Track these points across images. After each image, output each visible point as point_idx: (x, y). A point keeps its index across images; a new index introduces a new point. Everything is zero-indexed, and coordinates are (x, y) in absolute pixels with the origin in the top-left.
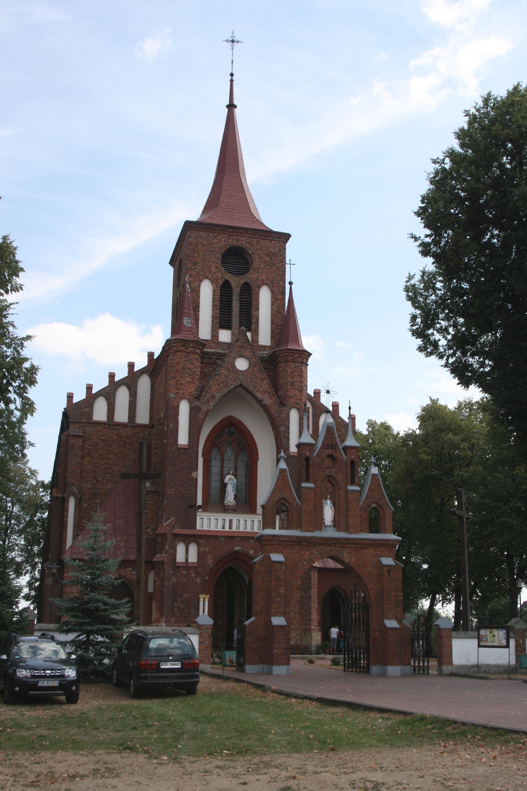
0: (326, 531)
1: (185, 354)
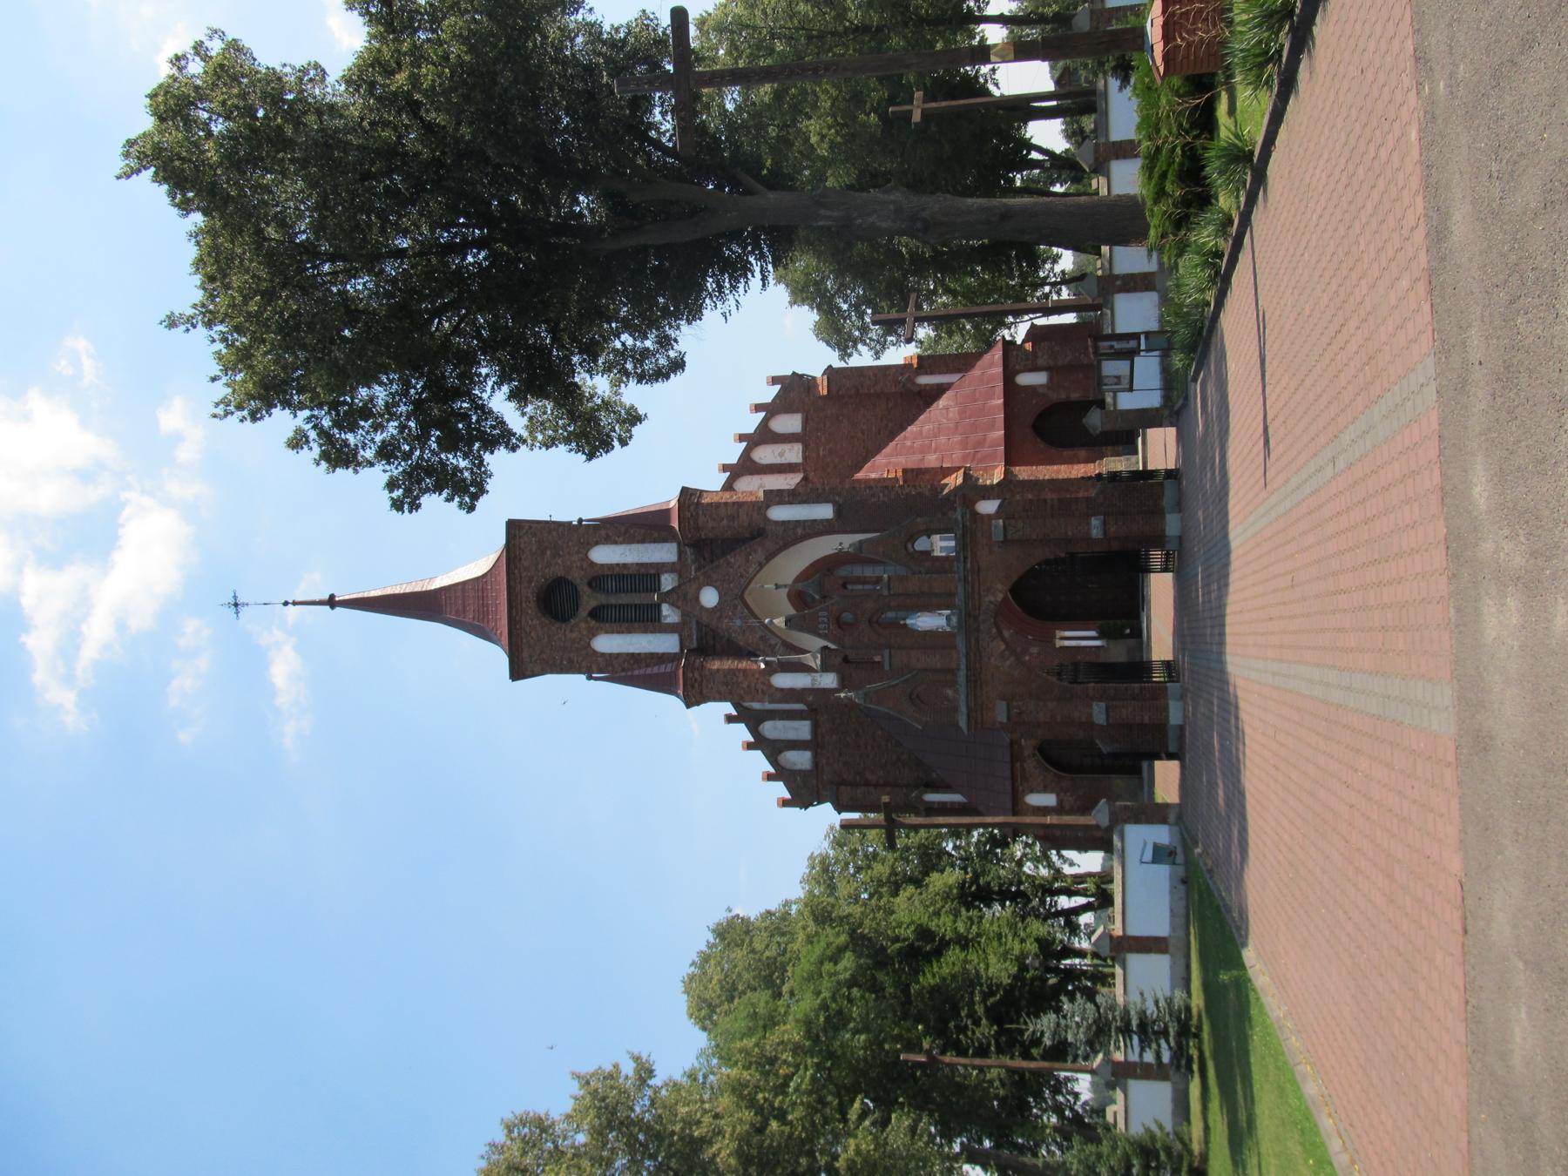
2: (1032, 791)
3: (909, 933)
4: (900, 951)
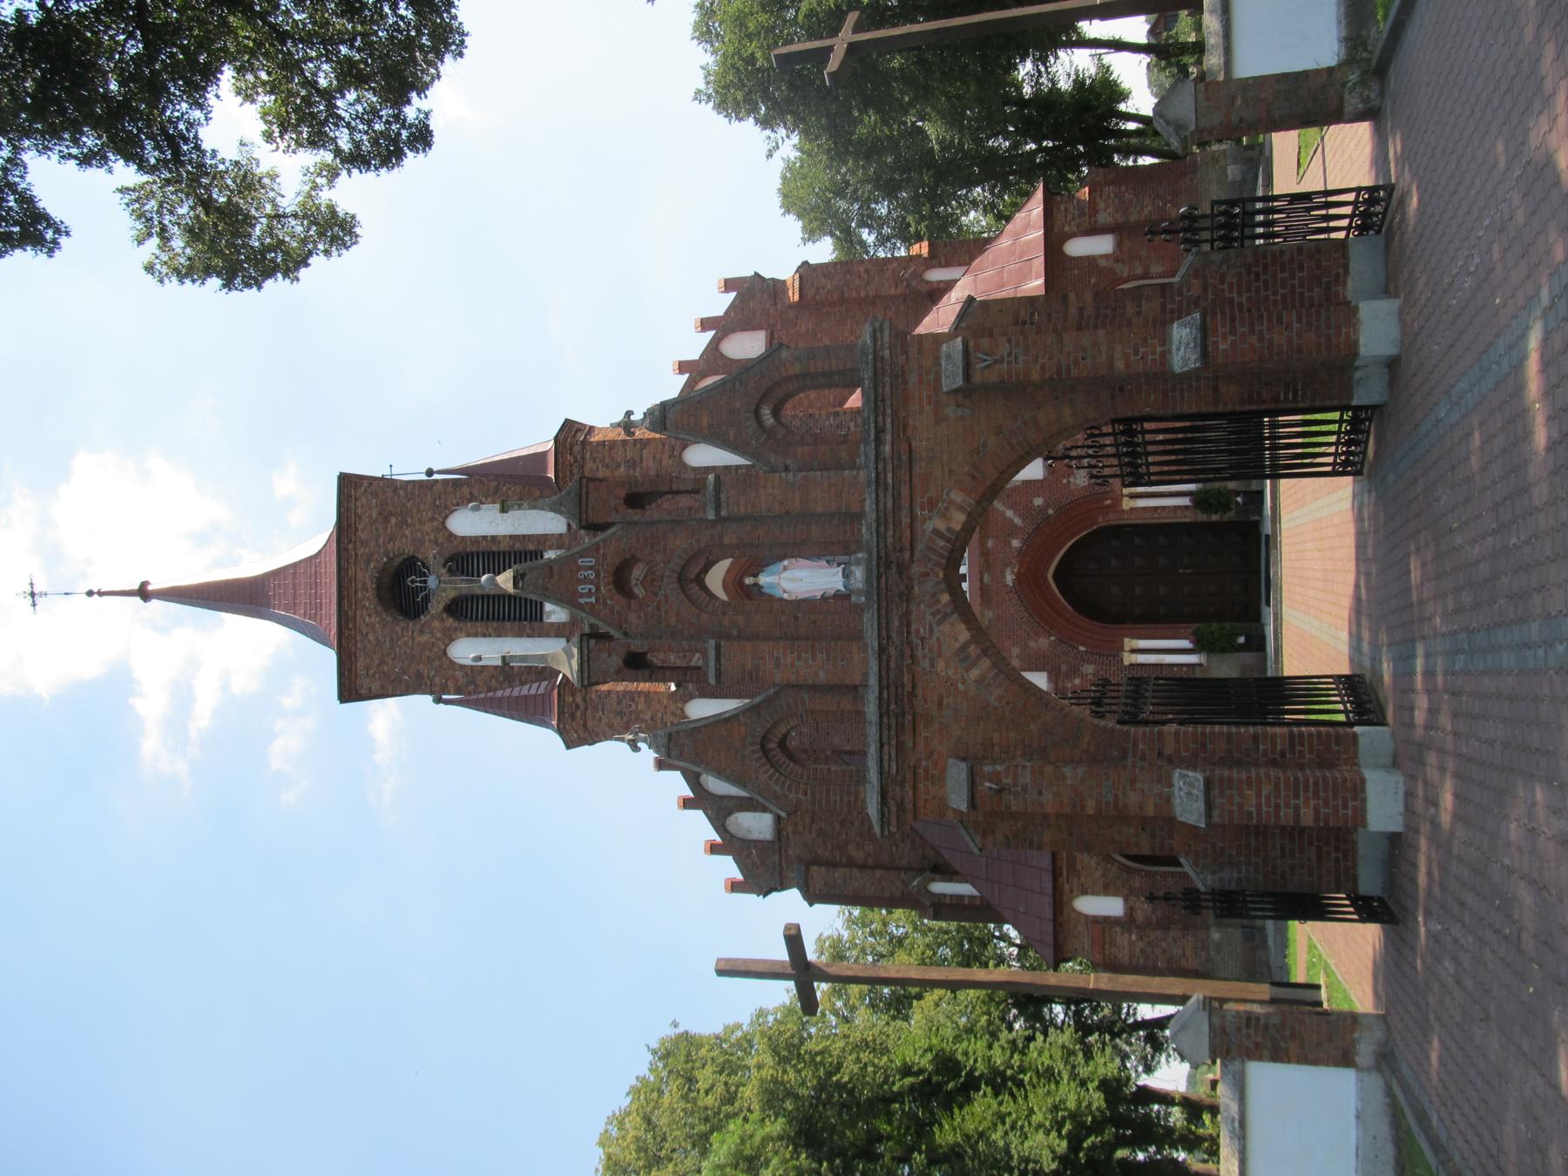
1: (589, 712)
2: (1084, 892)
3: (926, 1062)
4: (912, 1088)
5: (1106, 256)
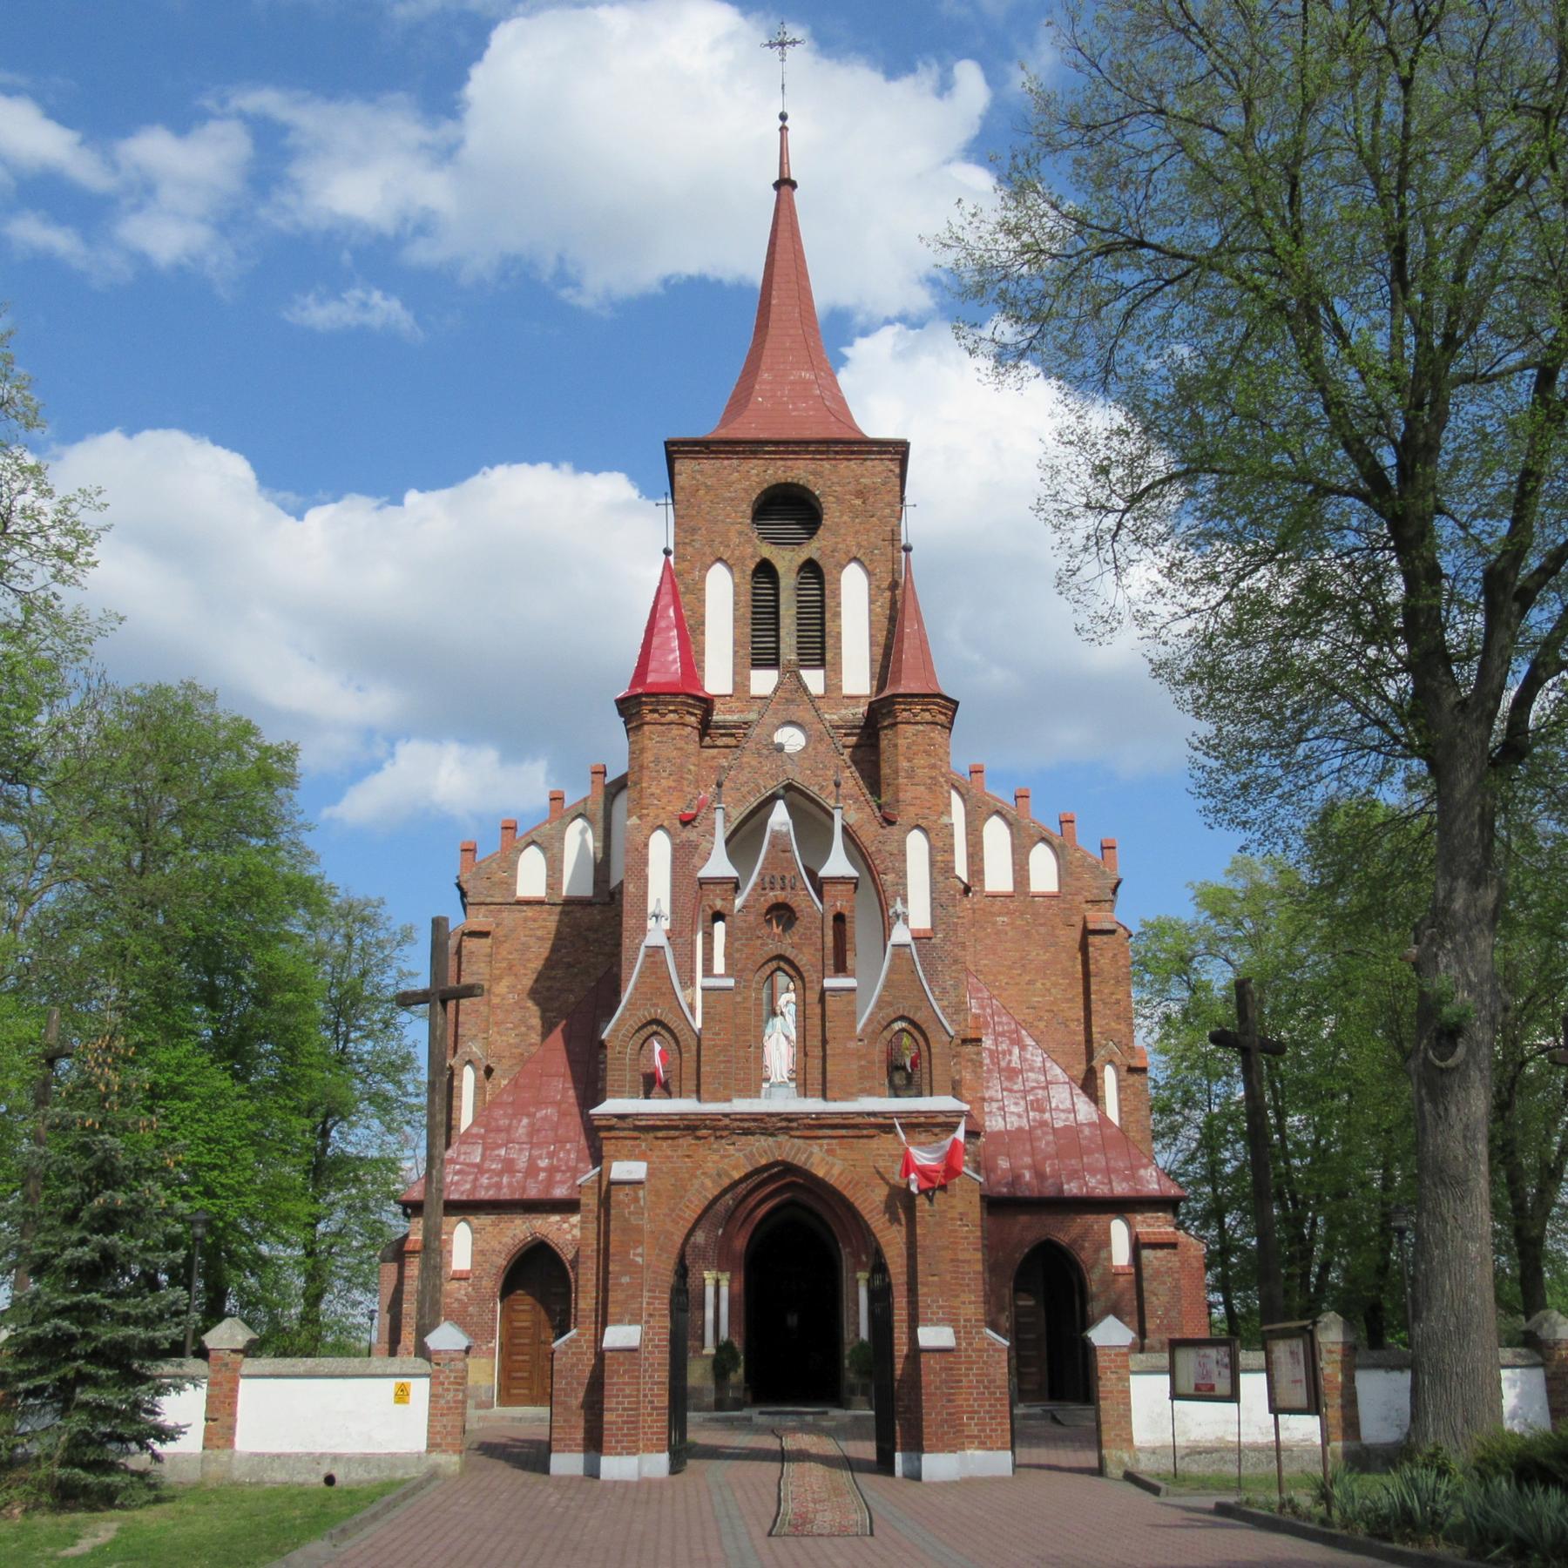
0: (769, 1096)
5: (1110, 1258)
